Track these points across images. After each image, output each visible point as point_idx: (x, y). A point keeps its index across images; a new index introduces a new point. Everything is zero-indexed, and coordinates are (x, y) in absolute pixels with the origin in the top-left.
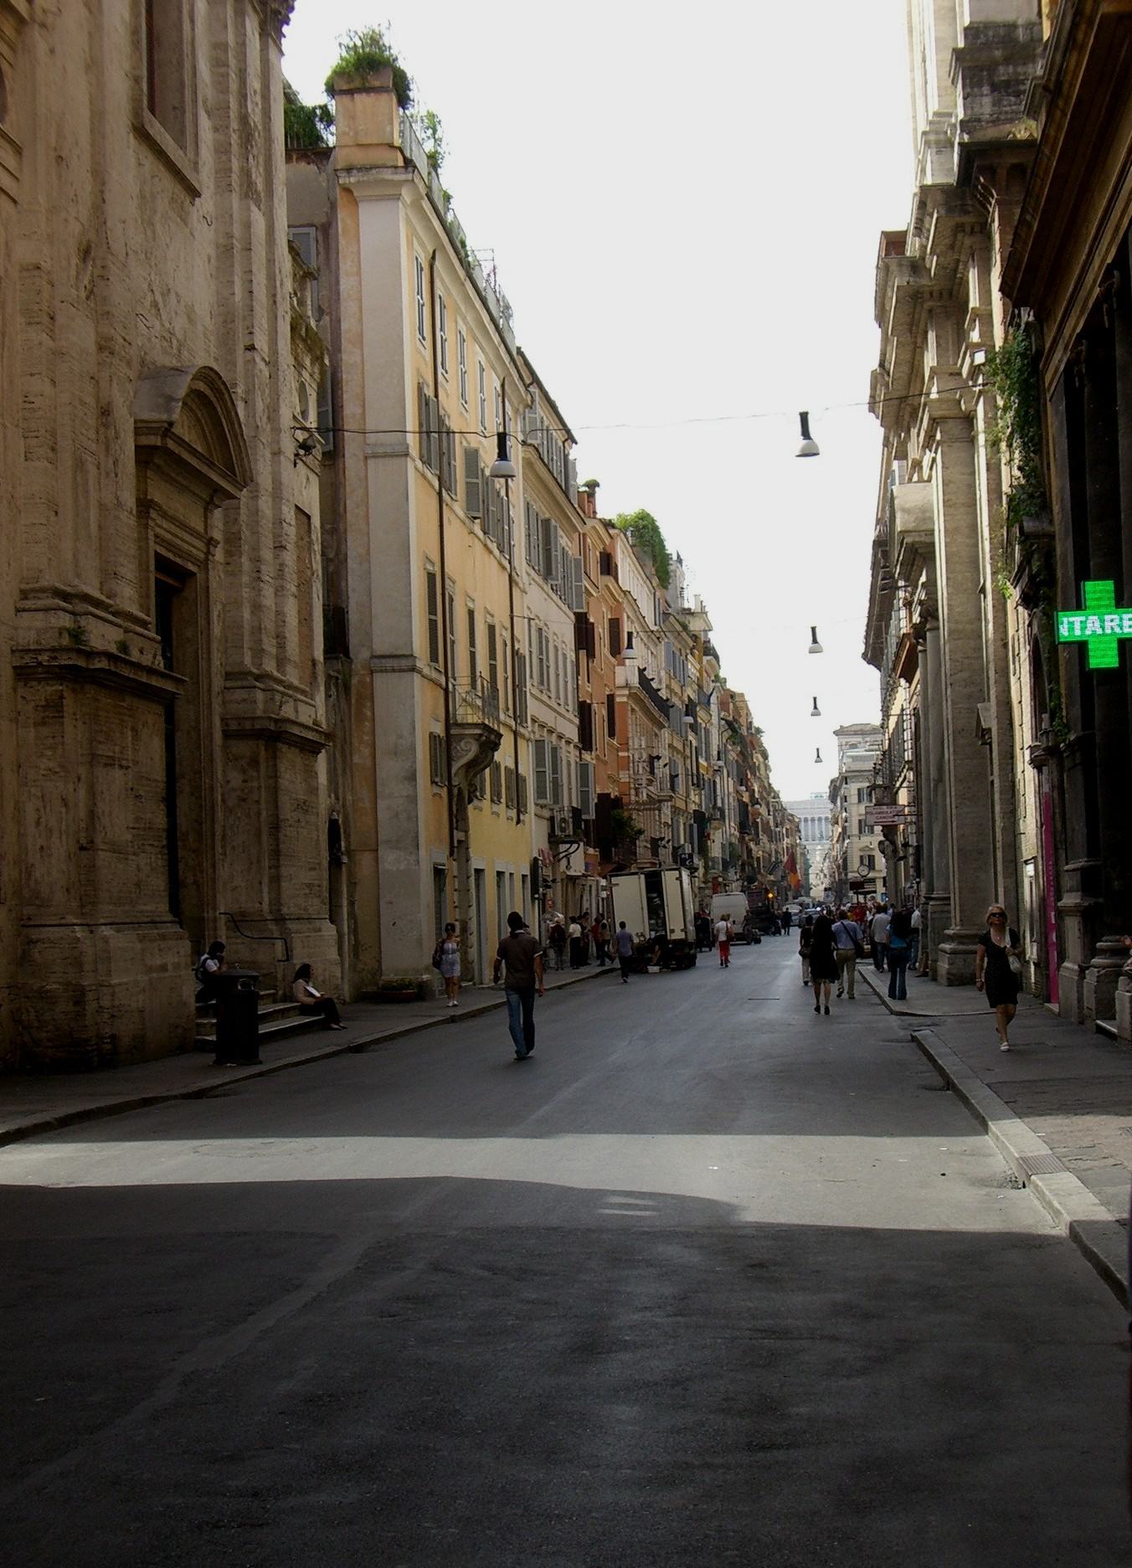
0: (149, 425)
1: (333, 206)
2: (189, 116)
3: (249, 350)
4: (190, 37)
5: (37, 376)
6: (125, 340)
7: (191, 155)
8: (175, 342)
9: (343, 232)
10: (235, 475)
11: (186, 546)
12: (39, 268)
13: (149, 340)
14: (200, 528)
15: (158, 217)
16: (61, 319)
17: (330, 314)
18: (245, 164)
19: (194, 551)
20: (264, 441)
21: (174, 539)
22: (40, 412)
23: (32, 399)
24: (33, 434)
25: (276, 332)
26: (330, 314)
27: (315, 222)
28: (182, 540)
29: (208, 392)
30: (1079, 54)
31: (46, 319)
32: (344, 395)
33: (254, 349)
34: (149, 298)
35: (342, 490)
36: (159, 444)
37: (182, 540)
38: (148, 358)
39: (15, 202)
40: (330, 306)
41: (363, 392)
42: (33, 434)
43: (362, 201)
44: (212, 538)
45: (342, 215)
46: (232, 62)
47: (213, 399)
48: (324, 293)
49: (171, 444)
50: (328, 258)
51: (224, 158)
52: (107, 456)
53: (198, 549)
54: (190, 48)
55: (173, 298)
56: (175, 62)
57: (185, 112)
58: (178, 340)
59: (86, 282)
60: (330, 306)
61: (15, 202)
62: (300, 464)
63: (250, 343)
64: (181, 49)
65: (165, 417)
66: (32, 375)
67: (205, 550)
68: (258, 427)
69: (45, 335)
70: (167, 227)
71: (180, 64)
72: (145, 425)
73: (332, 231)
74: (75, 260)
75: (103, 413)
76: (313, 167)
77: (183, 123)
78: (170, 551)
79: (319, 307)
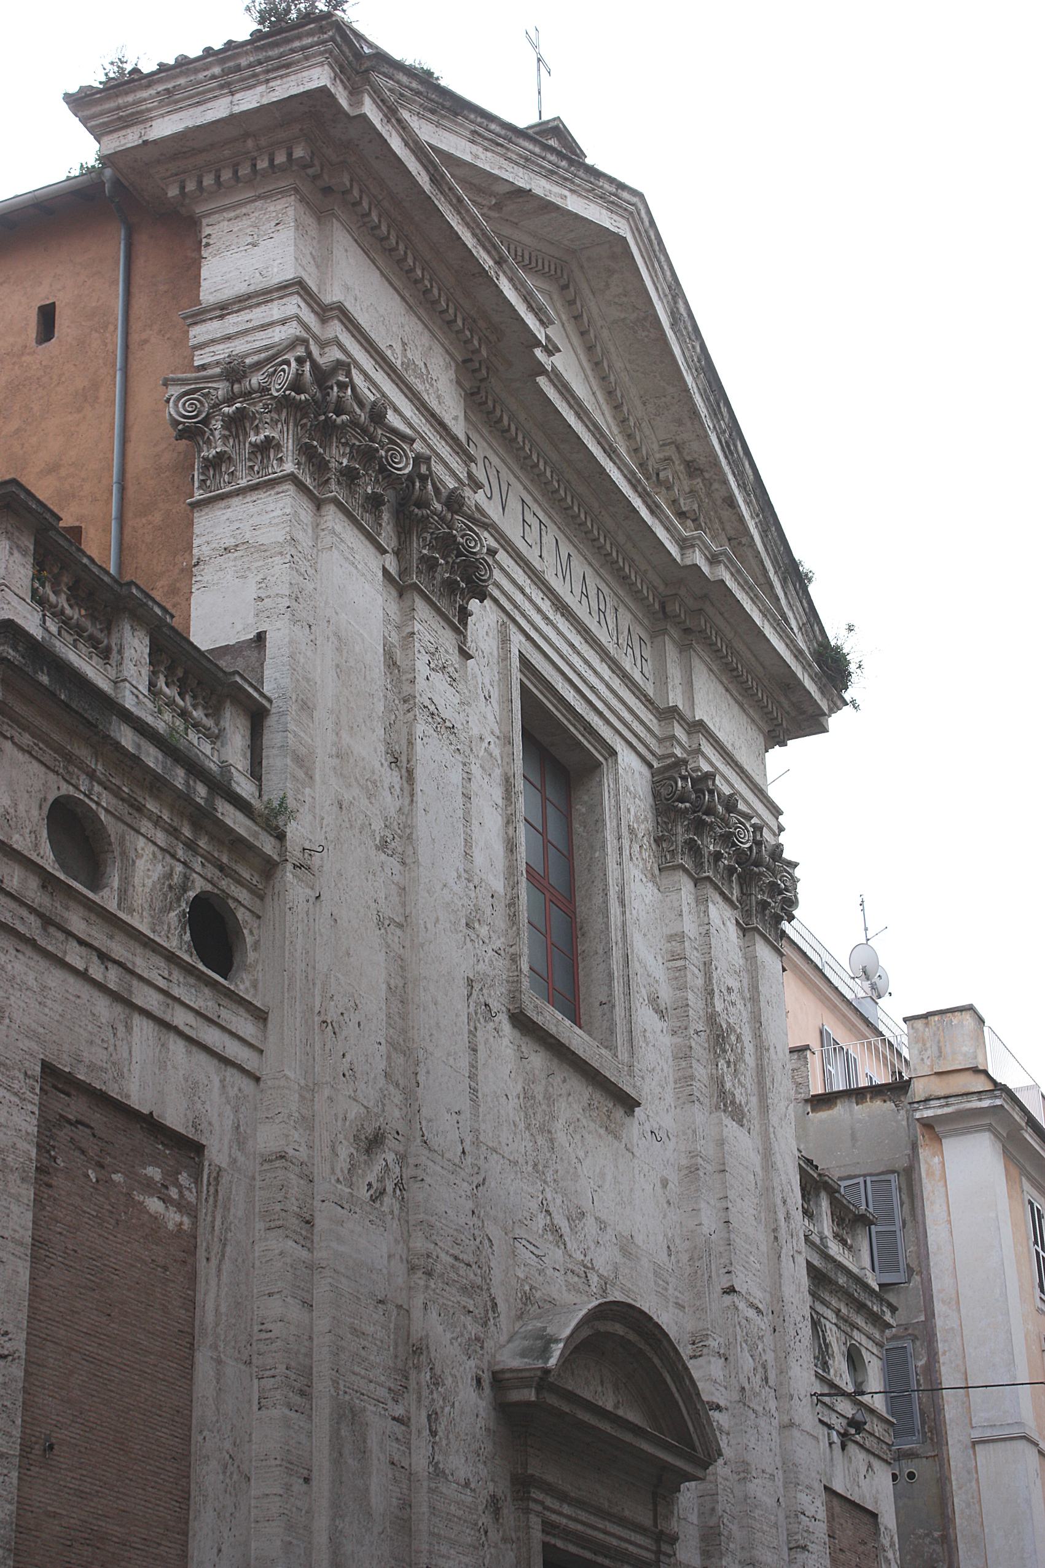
0: (520, 1375)
1: (914, 1147)
2: (619, 1012)
3: (728, 1293)
4: (619, 924)
5: (277, 1296)
6: (456, 1258)
7: (623, 1054)
8: (594, 1279)
9: (927, 1175)
10: (694, 1449)
11: (615, 1542)
12: (282, 1157)
13: (541, 1272)
14: (648, 1522)
15: (559, 1125)
16: (321, 1223)
17: (920, 1273)
18: (714, 1071)
19: (631, 1548)
20: (756, 1408)
21: (590, 1531)
22: (279, 1343)
23: (268, 1326)
24: (268, 1373)
25: (780, 1276)
26: (920, 1273)
27: (897, 1167)
28: (606, 1532)
29: (632, 1336)
30: (485, 526)
31: (294, 1223)
32: (942, 1368)
33: (735, 1291)
34: (541, 1220)
35: (948, 1488)
36: (533, 1399)
37: (606, 1532)
38: (538, 1295)
39: (257, 1080)
40: (919, 1265)
41: (964, 1363)
42: (268, 1373)
43: (945, 1137)
44: (661, 1532)
45: (924, 1153)
46: (695, 957)
47: (642, 1345)
48: (912, 1248)
49: (552, 1400)
50: (913, 1209)
51: (684, 1064)
52: (419, 1408)
53: (647, 1549)
54: (619, 934)
55: (590, 1225)
56: (601, 952)
57: (613, 1006)
58: (600, 1276)
59: (371, 1178)
60: (919, 1265)
61: (257, 1080)
62: (852, 1448)
63: (729, 1284)
64: (608, 935)
65: (540, 1364)
66: (270, 1295)
67: (654, 1548)
68: (743, 1388)
69: (291, 1243)
70: (578, 1137)
71: (608, 953)
72: (515, 1375)
73: (915, 1176)
74: (345, 1151)
75: (414, 1352)
76: (890, 1105)
77: (612, 1021)
78: (583, 1548)
79: (908, 1265)
